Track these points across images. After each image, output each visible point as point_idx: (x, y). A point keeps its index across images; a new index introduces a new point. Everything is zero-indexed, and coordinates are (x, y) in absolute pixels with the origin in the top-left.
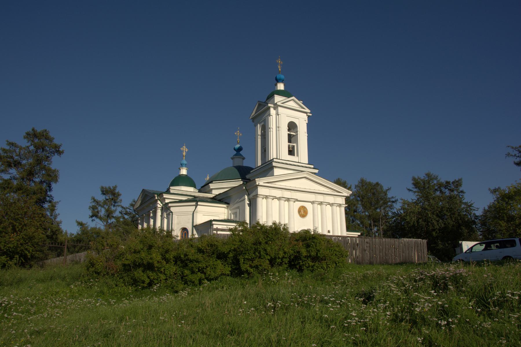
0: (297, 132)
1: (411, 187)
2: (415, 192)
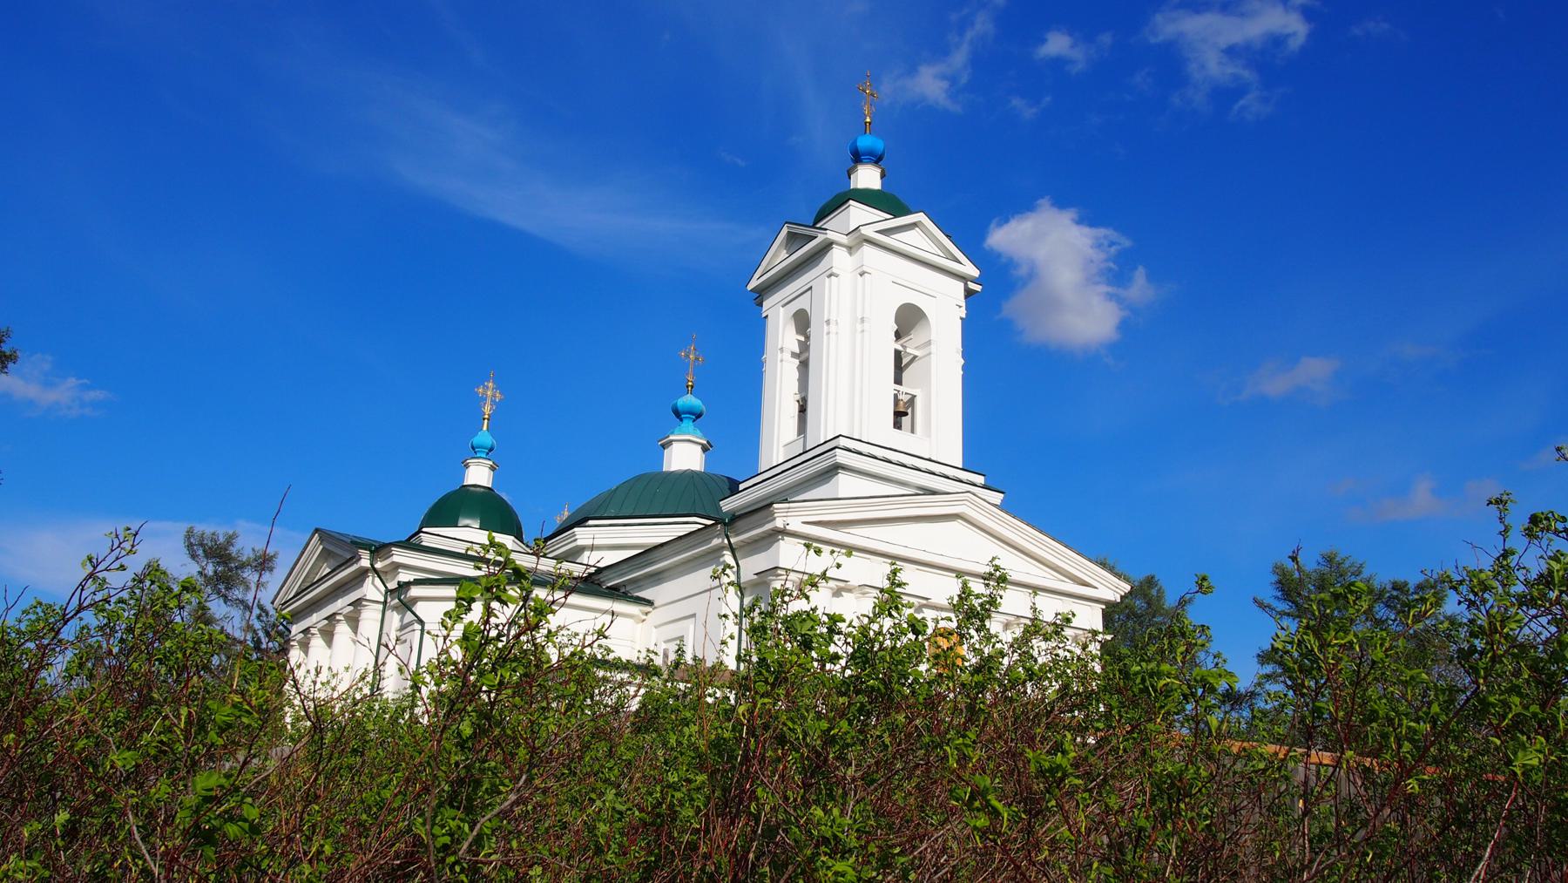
0: (929, 343)
1: (1269, 594)
2: (1282, 614)
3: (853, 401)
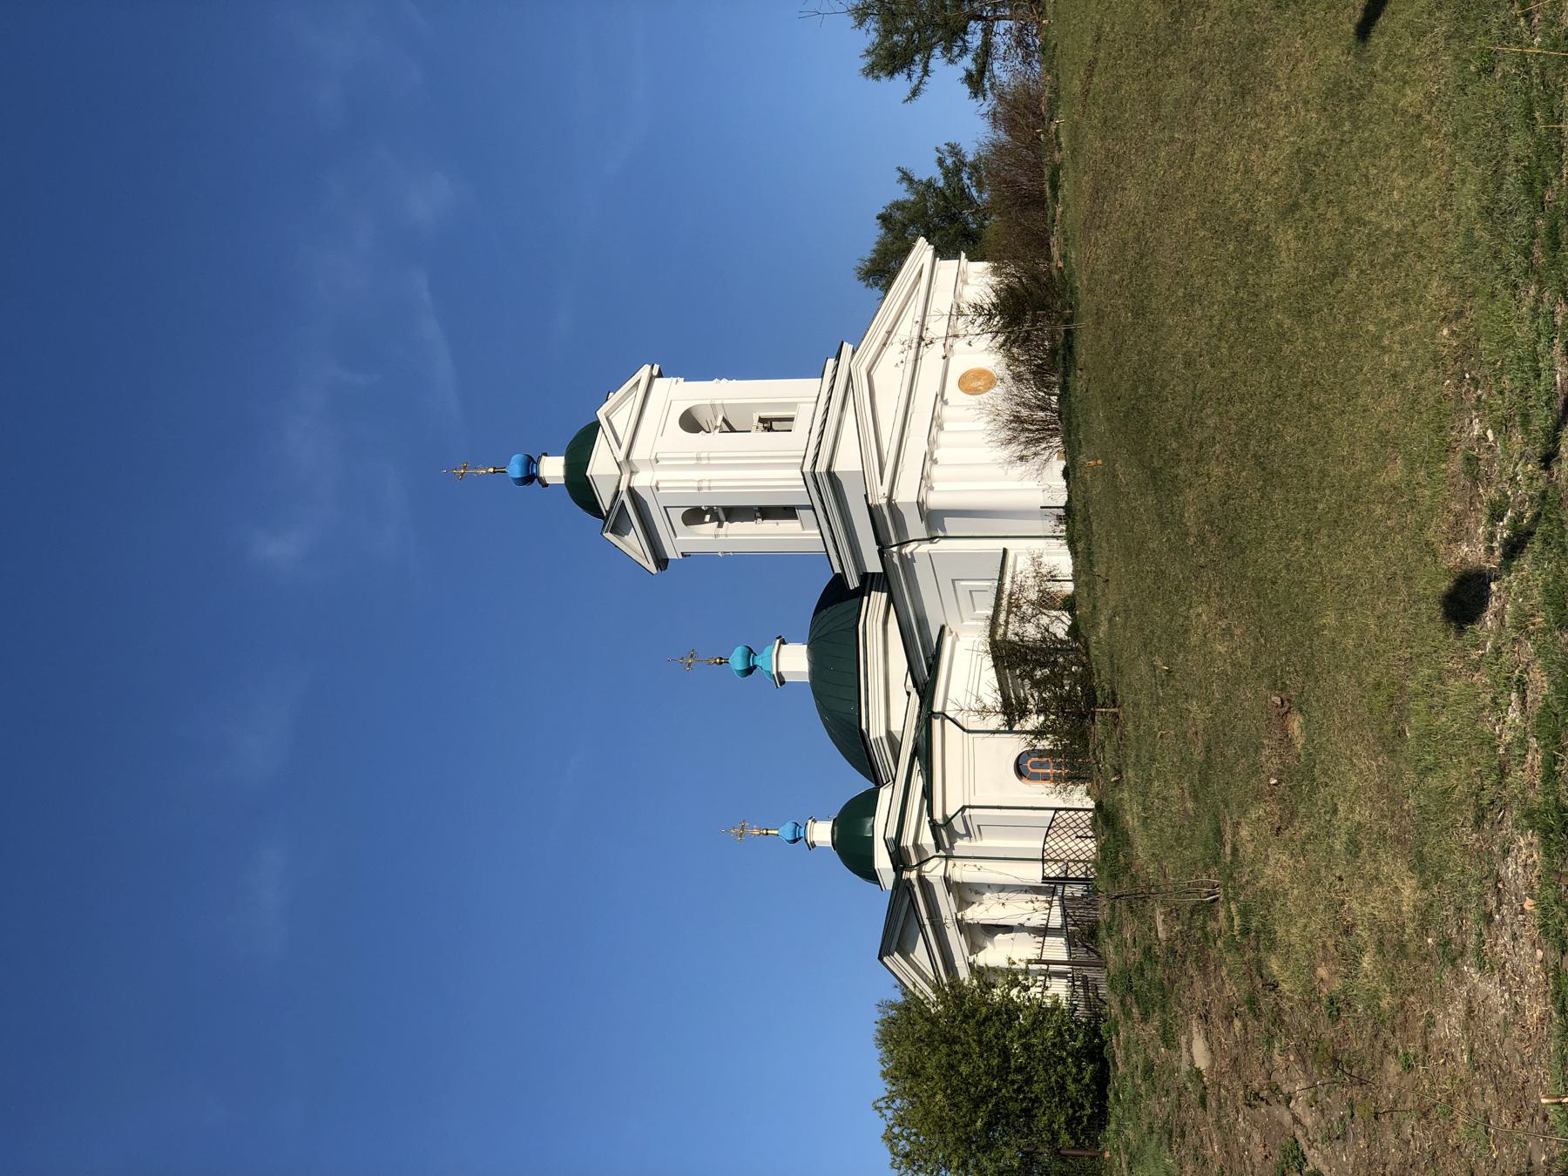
0: (713, 406)
1: (901, 83)
3: (772, 469)
